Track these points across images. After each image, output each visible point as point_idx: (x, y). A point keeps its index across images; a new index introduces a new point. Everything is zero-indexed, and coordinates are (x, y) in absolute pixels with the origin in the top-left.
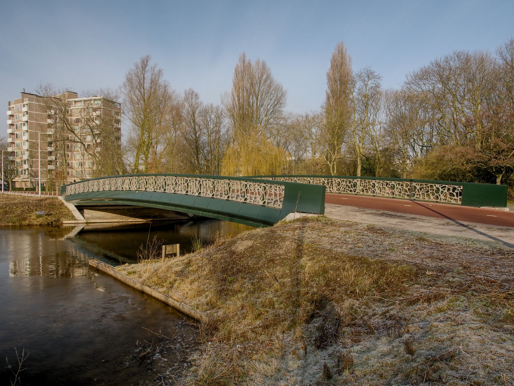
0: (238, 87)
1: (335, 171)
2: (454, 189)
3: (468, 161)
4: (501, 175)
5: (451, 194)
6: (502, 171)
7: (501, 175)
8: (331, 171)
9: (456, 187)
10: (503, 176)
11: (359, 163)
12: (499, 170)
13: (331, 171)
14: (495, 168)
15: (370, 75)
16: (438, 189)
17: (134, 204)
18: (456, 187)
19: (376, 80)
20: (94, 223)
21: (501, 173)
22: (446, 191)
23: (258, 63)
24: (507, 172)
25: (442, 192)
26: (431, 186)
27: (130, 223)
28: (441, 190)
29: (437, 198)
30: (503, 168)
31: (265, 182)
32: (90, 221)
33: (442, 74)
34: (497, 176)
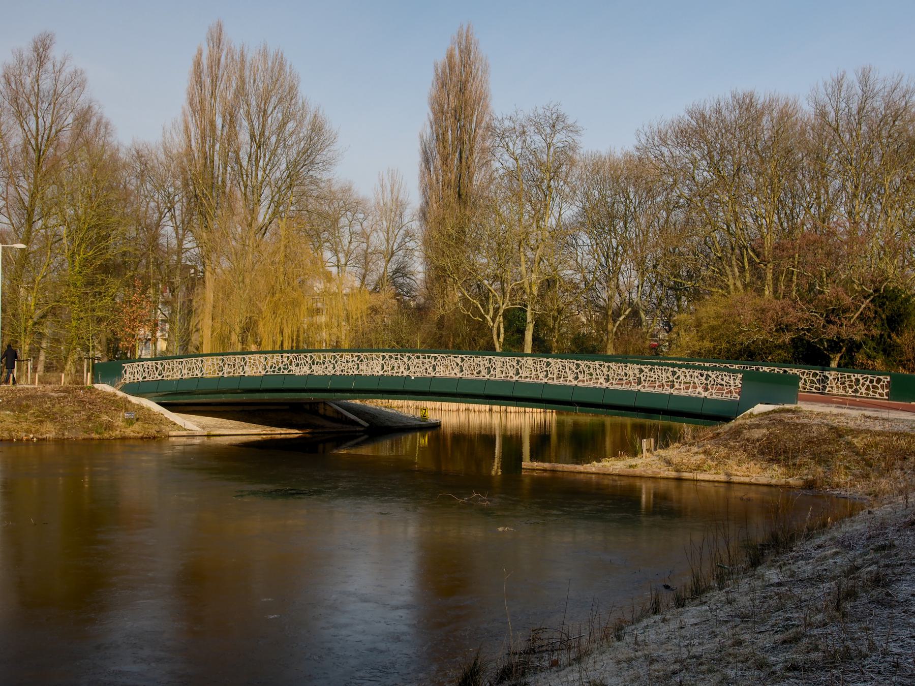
0: (198, 107)
1: (502, 336)
2: (879, 381)
3: (782, 328)
4: (839, 355)
5: (874, 387)
6: (841, 348)
7: (839, 355)
8: (495, 337)
9: (881, 377)
10: (841, 358)
11: (529, 319)
12: (835, 346)
13: (495, 337)
14: (828, 341)
15: (556, 122)
16: (857, 380)
17: (266, 397)
18: (881, 377)
19: (571, 134)
20: (220, 435)
21: (839, 351)
22: (867, 383)
23: (264, 55)
24: (850, 351)
25: (863, 385)
26: (849, 377)
27: (278, 437)
28: (861, 381)
29: (856, 391)
30: (843, 341)
31: (674, 366)
32: (214, 433)
33: (697, 132)
34: (832, 356)
